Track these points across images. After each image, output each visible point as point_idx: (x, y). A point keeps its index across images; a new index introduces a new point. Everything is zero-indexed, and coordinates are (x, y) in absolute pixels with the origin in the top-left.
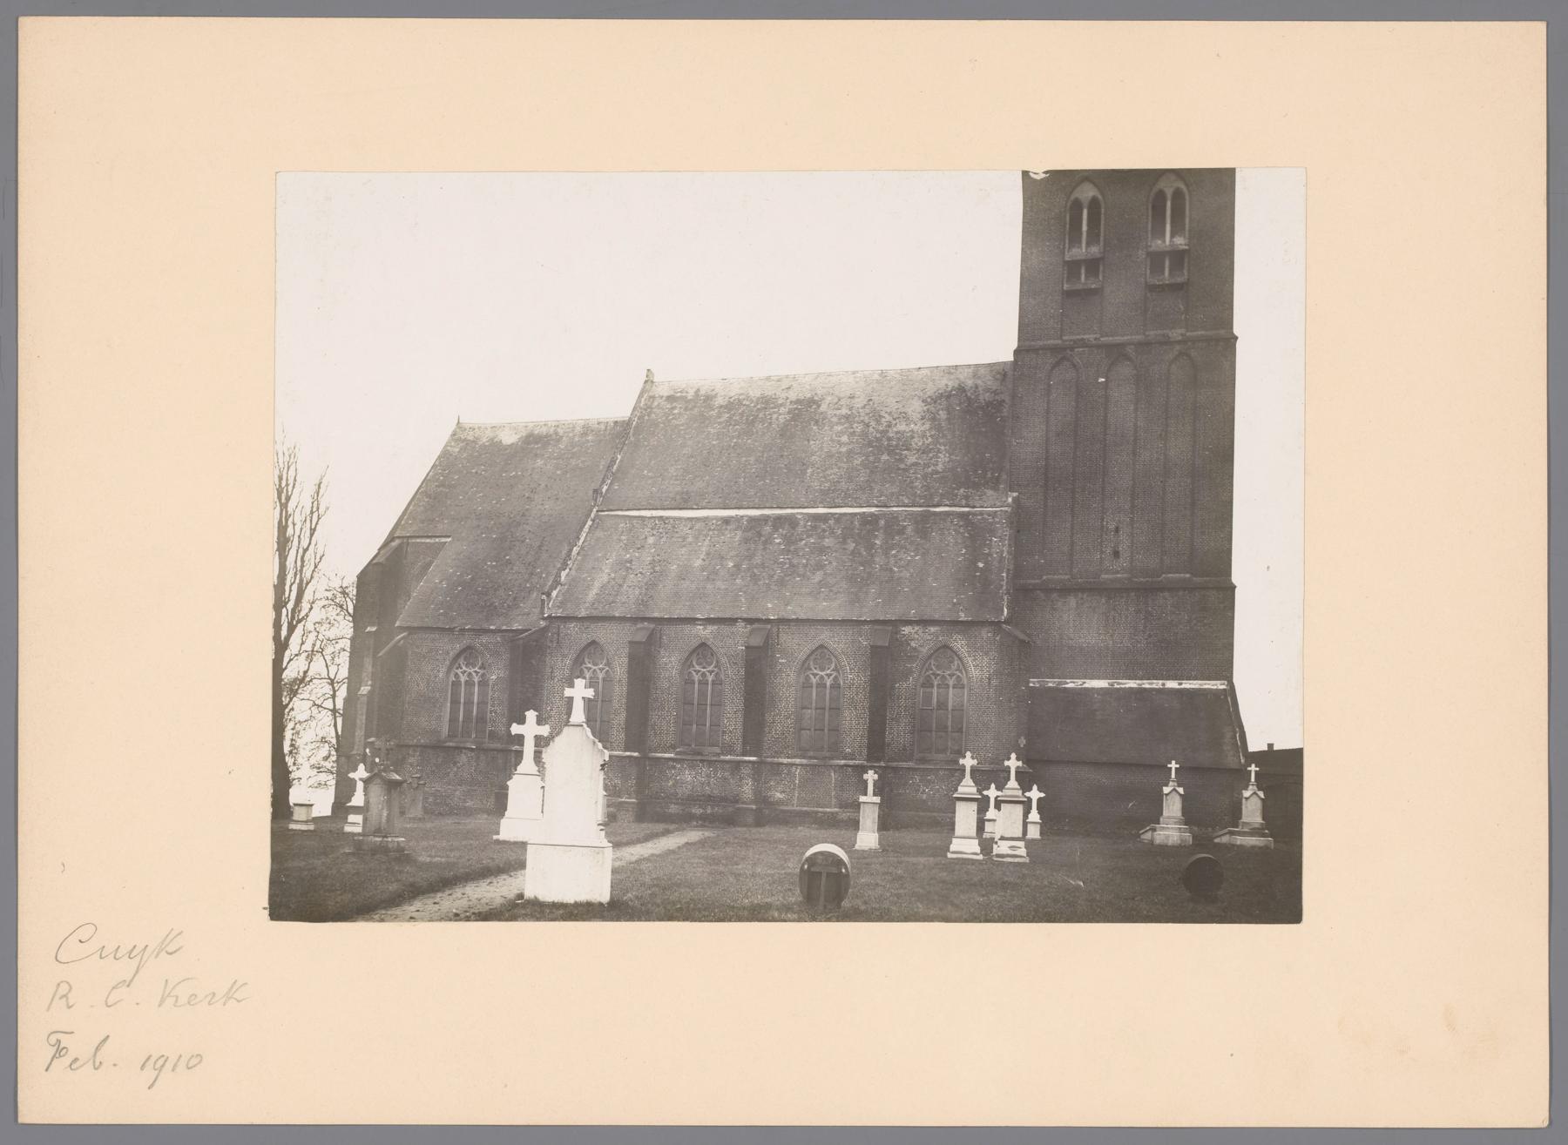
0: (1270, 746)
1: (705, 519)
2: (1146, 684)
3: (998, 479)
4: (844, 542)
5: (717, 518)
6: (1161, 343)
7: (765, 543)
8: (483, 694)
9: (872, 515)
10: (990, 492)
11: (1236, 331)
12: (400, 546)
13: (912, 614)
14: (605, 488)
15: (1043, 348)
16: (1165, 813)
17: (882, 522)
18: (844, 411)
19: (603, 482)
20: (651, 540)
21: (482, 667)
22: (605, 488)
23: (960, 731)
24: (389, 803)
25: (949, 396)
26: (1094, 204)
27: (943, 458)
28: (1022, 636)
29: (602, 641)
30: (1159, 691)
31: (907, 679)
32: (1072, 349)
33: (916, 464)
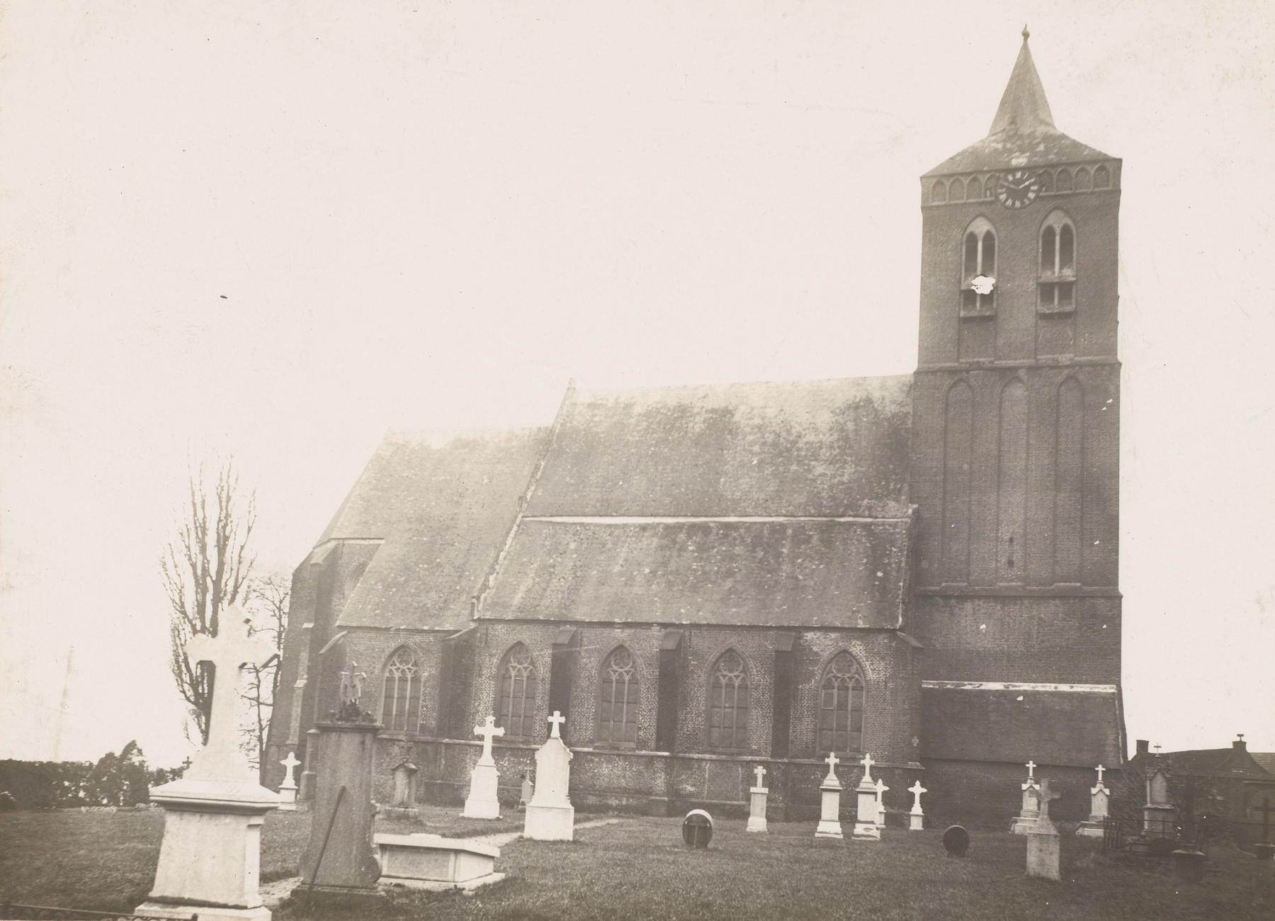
0: (1240, 745)
1: (625, 526)
2: (1040, 687)
3: (900, 490)
4: (753, 551)
5: (635, 526)
6: (1052, 368)
7: (680, 550)
8: (415, 689)
9: (781, 524)
10: (892, 504)
11: (1120, 358)
12: (335, 550)
13: (815, 621)
14: (529, 494)
15: (940, 370)
16: (1025, 807)
17: (790, 531)
18: (757, 421)
19: (528, 488)
20: (573, 546)
21: (415, 664)
22: (529, 494)
23: (859, 730)
24: (409, 784)
25: (857, 408)
26: (988, 237)
27: (849, 469)
28: (915, 643)
29: (527, 642)
30: (1051, 694)
31: (809, 681)
32: (968, 371)
33: (824, 474)
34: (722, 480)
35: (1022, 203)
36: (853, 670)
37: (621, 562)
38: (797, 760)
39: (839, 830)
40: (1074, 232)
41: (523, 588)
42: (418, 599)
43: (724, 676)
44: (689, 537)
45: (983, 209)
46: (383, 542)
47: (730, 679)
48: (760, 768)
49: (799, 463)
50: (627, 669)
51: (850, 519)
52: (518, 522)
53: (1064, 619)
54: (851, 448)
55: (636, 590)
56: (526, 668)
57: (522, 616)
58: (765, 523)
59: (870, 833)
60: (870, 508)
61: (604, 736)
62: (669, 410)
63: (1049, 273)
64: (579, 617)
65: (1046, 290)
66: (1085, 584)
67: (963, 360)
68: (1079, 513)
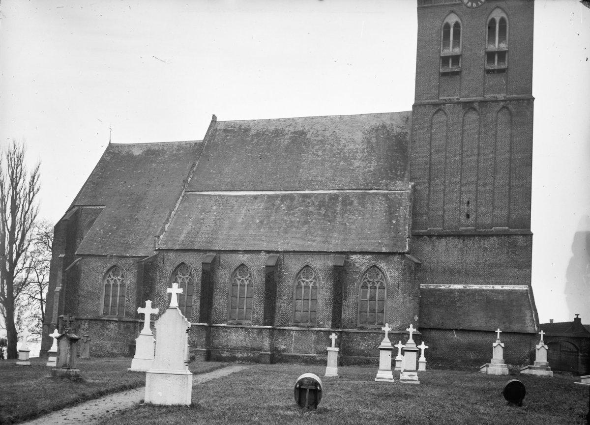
2: (484, 287)
3: (403, 175)
6: (493, 101)
7: (276, 209)
8: (122, 291)
9: (335, 194)
10: (399, 182)
12: (77, 212)
13: (357, 249)
15: (429, 104)
17: (340, 198)
18: (320, 138)
19: (189, 176)
20: (214, 208)
23: (382, 312)
24: (71, 349)
26: (457, 25)
30: (491, 291)
32: (444, 104)
34: (301, 170)
35: (477, 4)
36: (379, 277)
37: (242, 217)
38: (346, 330)
39: (391, 376)
40: (507, 22)
41: (185, 232)
42: (124, 239)
43: (303, 281)
44: (282, 201)
45: (454, 8)
46: (104, 207)
47: (307, 283)
48: (334, 334)
49: (345, 160)
50: (246, 278)
51: (376, 191)
52: (183, 194)
53: (498, 248)
54: (374, 152)
55: (251, 232)
56: (187, 278)
57: (184, 247)
58: (326, 194)
59: (413, 378)
60: (386, 185)
61: (233, 317)
62: (270, 132)
63: (492, 46)
64: (217, 248)
65: (490, 56)
66: (511, 228)
67: (440, 98)
68: (508, 187)
